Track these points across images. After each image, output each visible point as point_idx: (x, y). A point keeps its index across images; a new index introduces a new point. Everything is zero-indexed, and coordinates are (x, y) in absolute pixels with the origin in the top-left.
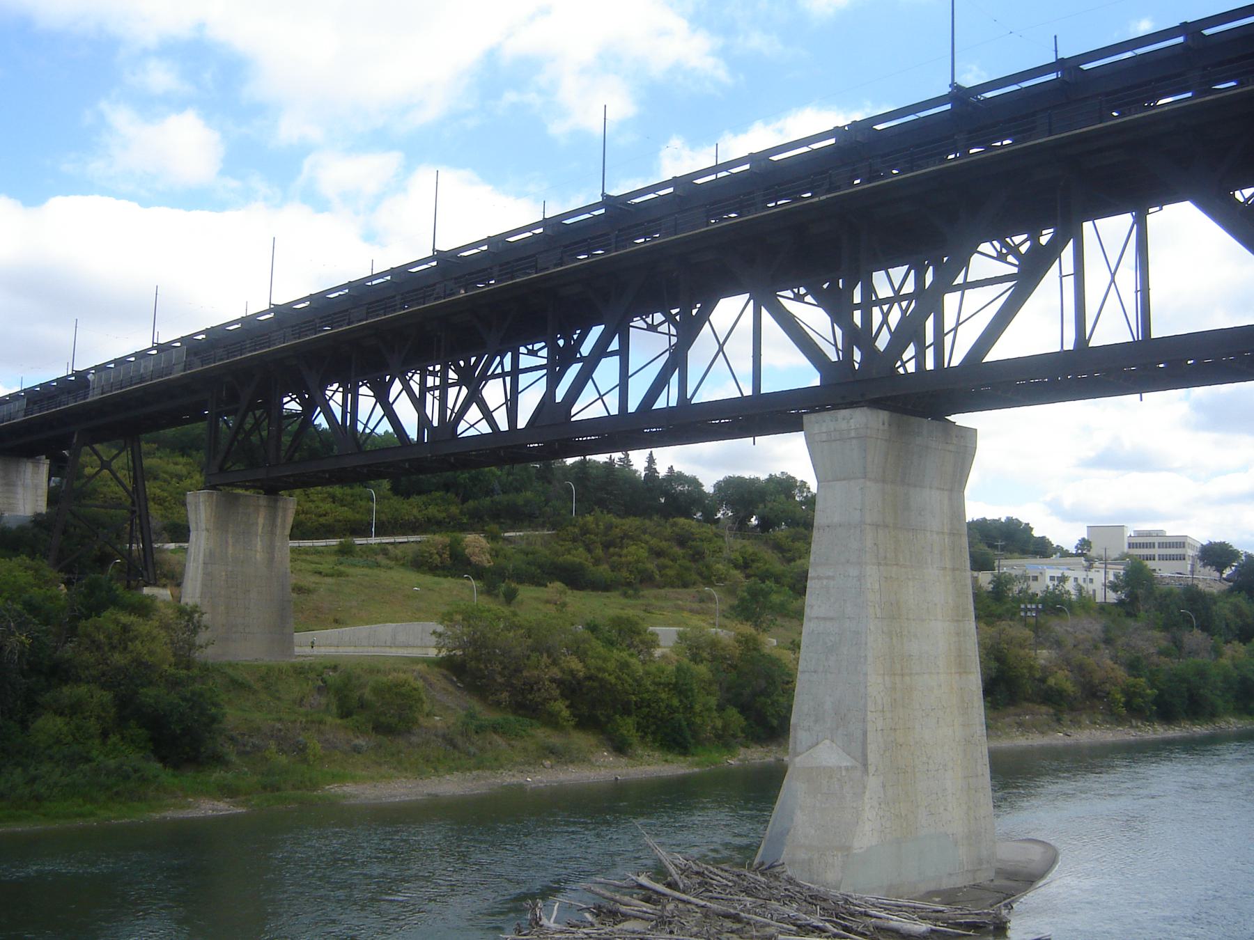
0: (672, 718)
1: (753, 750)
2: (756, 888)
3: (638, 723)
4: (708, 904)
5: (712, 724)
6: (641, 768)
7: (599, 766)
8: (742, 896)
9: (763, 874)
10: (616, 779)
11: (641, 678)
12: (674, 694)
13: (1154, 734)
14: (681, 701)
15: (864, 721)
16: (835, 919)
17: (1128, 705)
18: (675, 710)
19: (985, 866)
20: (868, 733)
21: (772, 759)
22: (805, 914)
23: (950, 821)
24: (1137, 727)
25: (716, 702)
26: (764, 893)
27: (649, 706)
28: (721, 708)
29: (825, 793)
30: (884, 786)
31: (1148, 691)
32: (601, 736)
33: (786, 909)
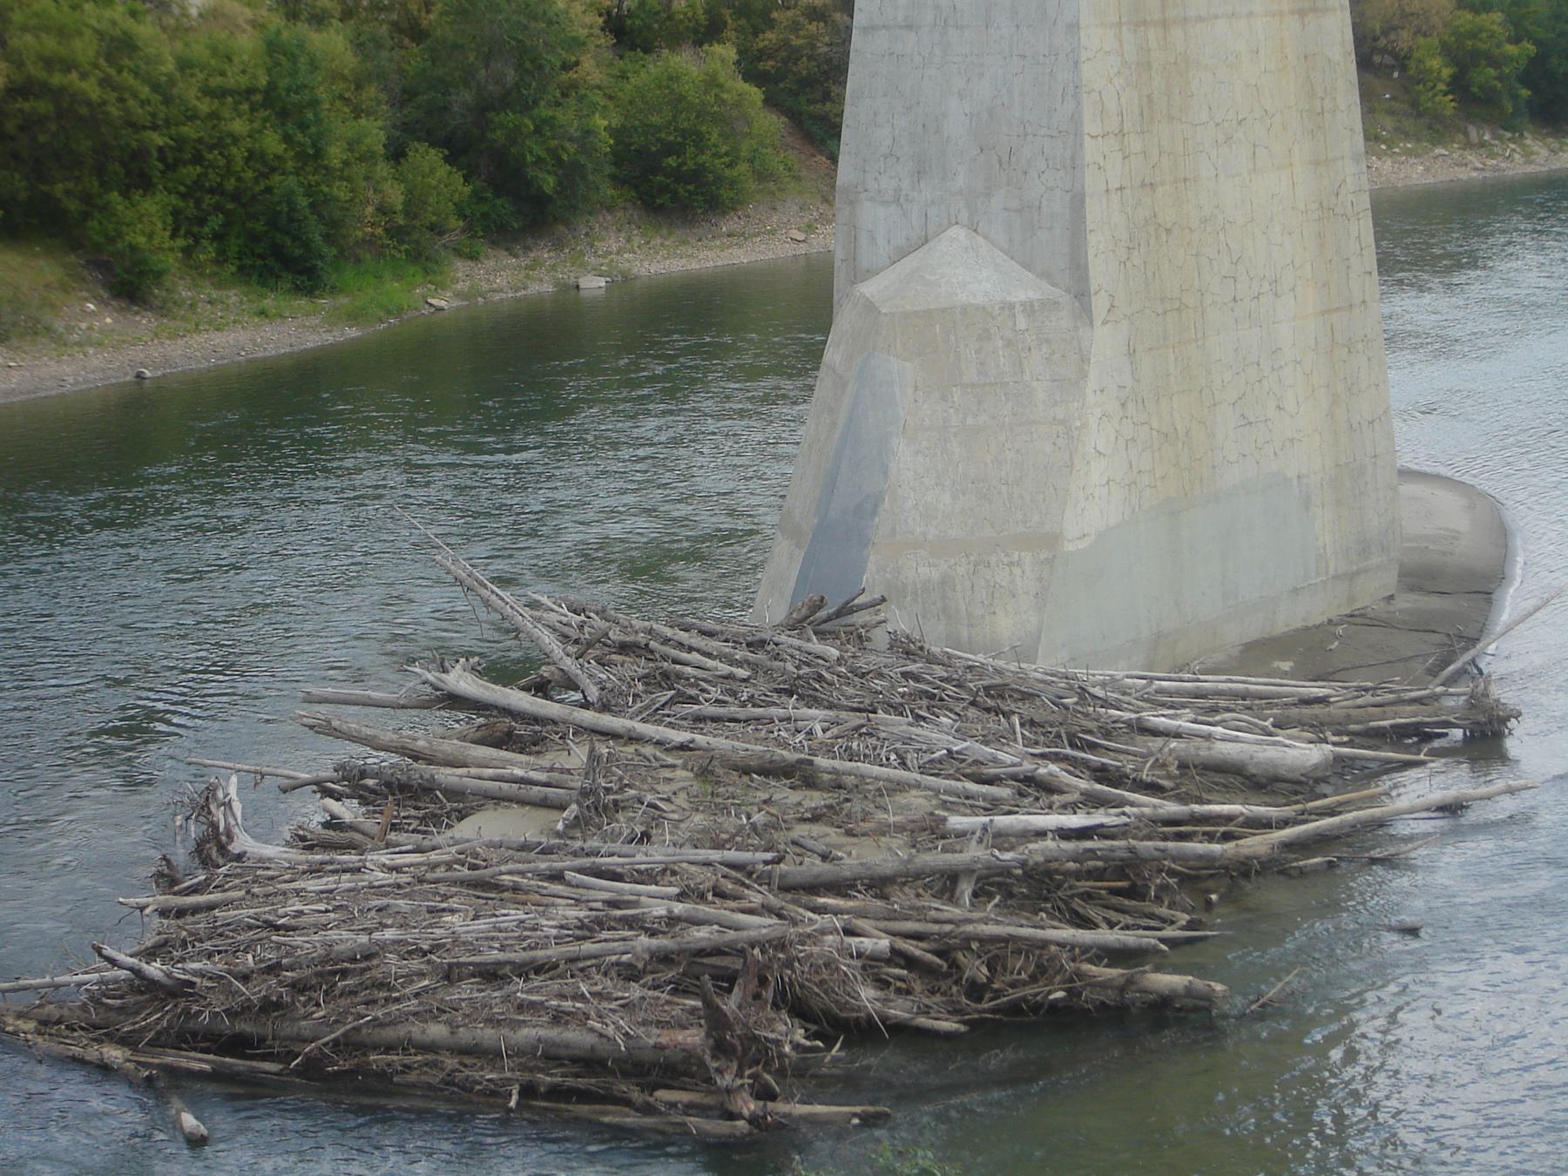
0: (268, 190)
1: (491, 263)
2: (820, 678)
3: (176, 213)
4: (700, 739)
5: (377, 199)
6: (201, 338)
7: (79, 344)
8: (791, 707)
9: (821, 635)
10: (139, 376)
11: (171, 81)
12: (265, 120)
13: (1529, 162)
14: (287, 139)
15: (1074, 164)
16: (1068, 751)
17: (1458, 85)
18: (272, 167)
19: (1376, 560)
20: (1087, 200)
21: (548, 288)
22: (986, 743)
23: (1292, 440)
24: (1482, 145)
25: (382, 137)
26: (850, 691)
27: (198, 159)
28: (396, 154)
29: (973, 385)
30: (1132, 353)
31: (1511, 49)
32: (72, 258)
33: (924, 732)
